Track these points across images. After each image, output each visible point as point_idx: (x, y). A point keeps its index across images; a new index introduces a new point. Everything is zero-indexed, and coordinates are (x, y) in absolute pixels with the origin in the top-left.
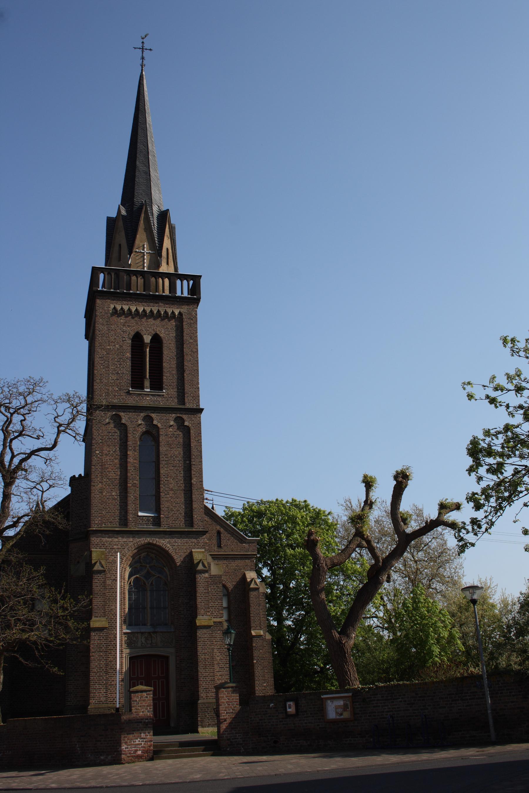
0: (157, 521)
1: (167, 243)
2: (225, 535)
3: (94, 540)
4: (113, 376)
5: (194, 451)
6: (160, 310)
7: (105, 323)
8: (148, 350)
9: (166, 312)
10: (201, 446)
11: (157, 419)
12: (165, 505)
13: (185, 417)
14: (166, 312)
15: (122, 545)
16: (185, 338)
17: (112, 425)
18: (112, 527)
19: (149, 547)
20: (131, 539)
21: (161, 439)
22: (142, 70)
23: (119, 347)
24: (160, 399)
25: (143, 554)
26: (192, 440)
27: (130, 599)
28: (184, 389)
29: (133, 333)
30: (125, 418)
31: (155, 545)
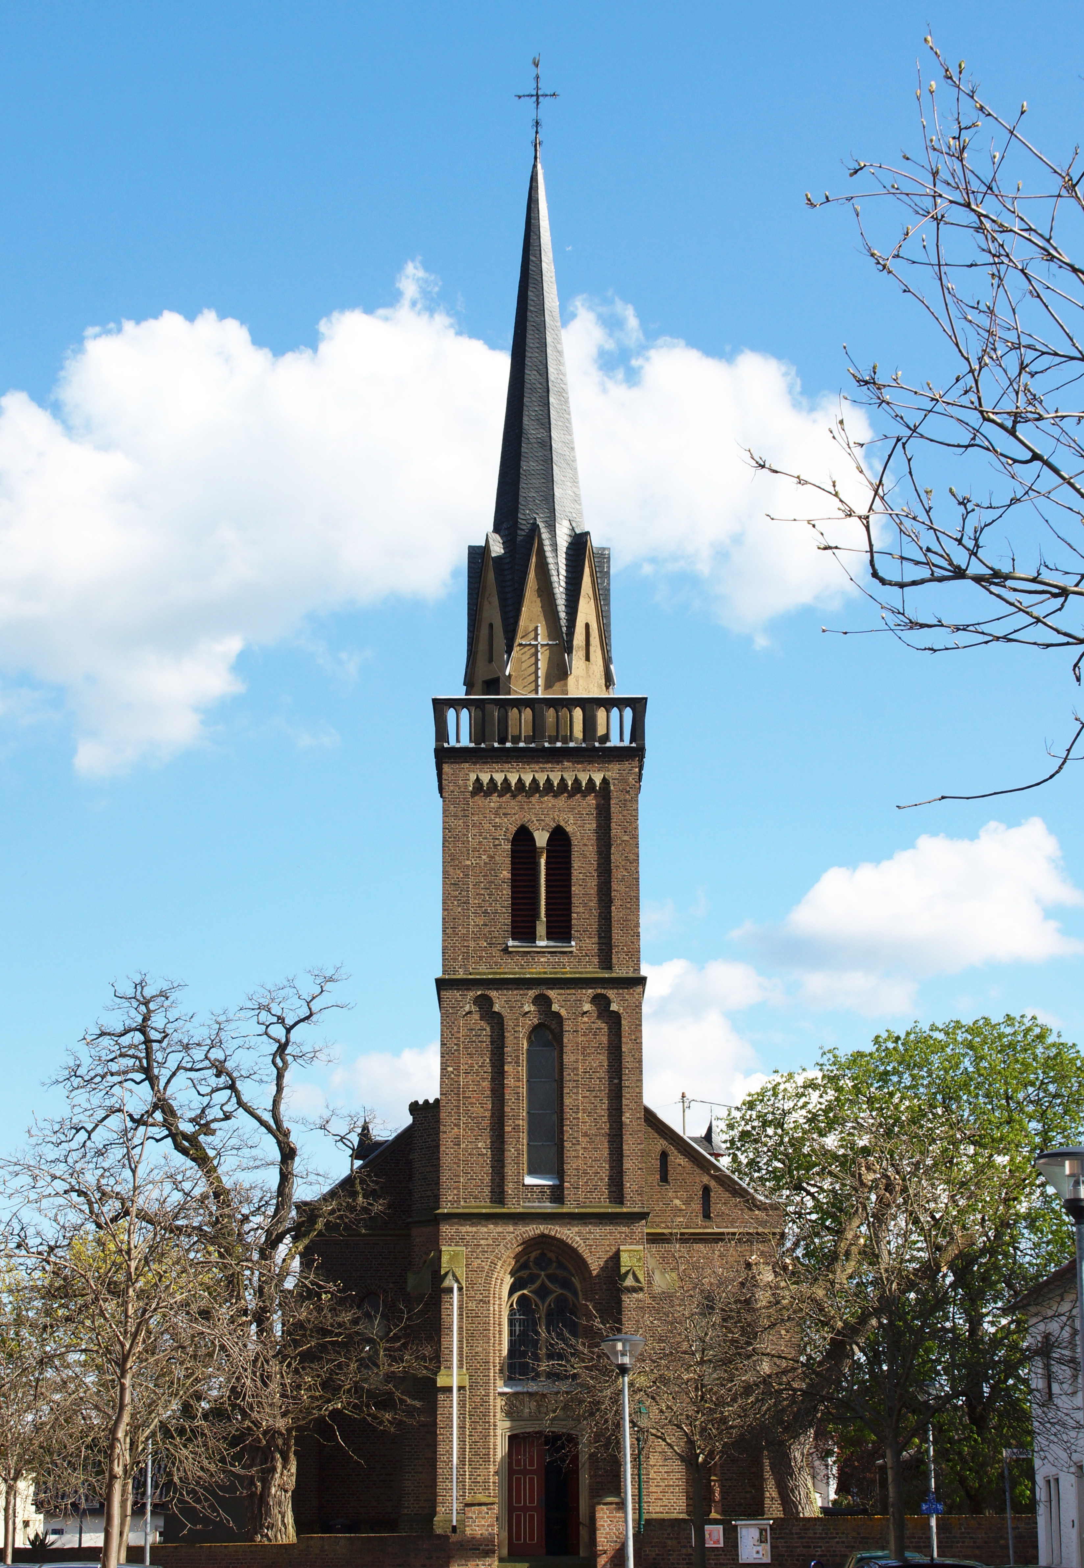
0: (557, 1194)
1: (586, 611)
2: (718, 1193)
3: (446, 1230)
4: (477, 920)
5: (627, 1061)
6: (566, 776)
7: (461, 814)
8: (543, 861)
9: (577, 781)
10: (640, 1050)
11: (559, 1001)
12: (571, 1166)
13: (611, 993)
14: (577, 781)
15: (495, 1240)
16: (613, 832)
17: (476, 1016)
18: (477, 1207)
19: (543, 1240)
20: (511, 1229)
21: (565, 1040)
22: (536, 158)
23: (487, 860)
24: (565, 959)
25: (534, 1253)
26: (624, 1040)
27: (511, 1333)
28: (610, 938)
29: (513, 829)
30: (500, 1001)
31: (554, 1238)
